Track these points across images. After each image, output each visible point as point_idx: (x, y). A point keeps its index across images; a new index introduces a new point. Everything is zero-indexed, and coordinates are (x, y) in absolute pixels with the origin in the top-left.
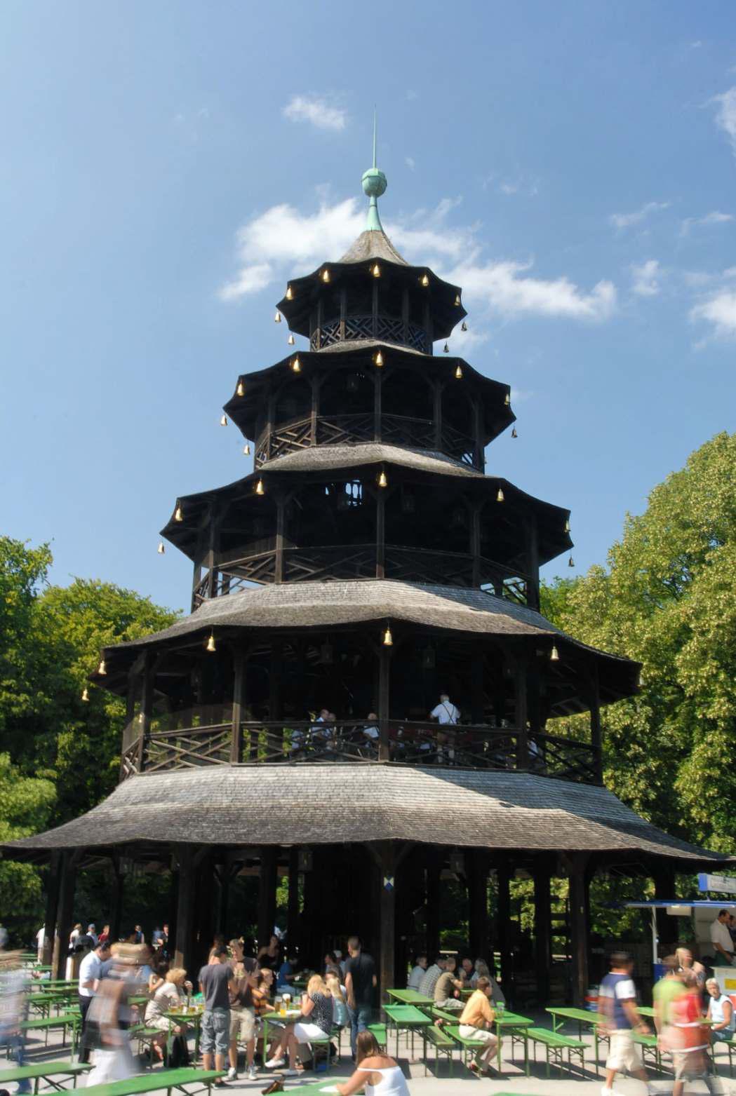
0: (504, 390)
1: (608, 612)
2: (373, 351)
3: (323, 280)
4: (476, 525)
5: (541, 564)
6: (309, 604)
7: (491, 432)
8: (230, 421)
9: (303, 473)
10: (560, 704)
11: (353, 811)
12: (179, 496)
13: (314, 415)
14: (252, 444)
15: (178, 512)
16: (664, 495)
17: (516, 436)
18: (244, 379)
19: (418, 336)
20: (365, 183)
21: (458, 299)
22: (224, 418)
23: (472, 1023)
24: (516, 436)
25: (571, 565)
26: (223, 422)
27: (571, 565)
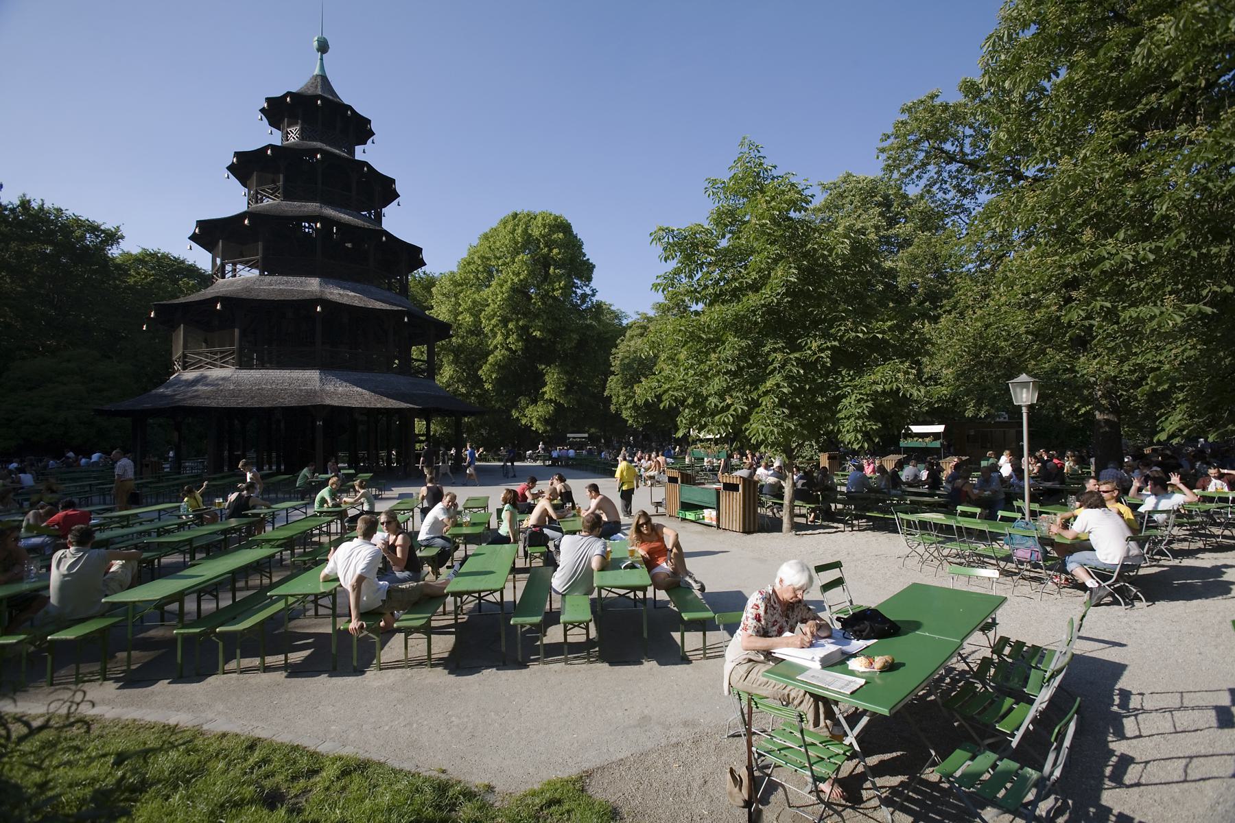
6: (277, 287)
9: (273, 216)
11: (301, 390)
16: (486, 237)
18: (237, 154)
23: (854, 603)
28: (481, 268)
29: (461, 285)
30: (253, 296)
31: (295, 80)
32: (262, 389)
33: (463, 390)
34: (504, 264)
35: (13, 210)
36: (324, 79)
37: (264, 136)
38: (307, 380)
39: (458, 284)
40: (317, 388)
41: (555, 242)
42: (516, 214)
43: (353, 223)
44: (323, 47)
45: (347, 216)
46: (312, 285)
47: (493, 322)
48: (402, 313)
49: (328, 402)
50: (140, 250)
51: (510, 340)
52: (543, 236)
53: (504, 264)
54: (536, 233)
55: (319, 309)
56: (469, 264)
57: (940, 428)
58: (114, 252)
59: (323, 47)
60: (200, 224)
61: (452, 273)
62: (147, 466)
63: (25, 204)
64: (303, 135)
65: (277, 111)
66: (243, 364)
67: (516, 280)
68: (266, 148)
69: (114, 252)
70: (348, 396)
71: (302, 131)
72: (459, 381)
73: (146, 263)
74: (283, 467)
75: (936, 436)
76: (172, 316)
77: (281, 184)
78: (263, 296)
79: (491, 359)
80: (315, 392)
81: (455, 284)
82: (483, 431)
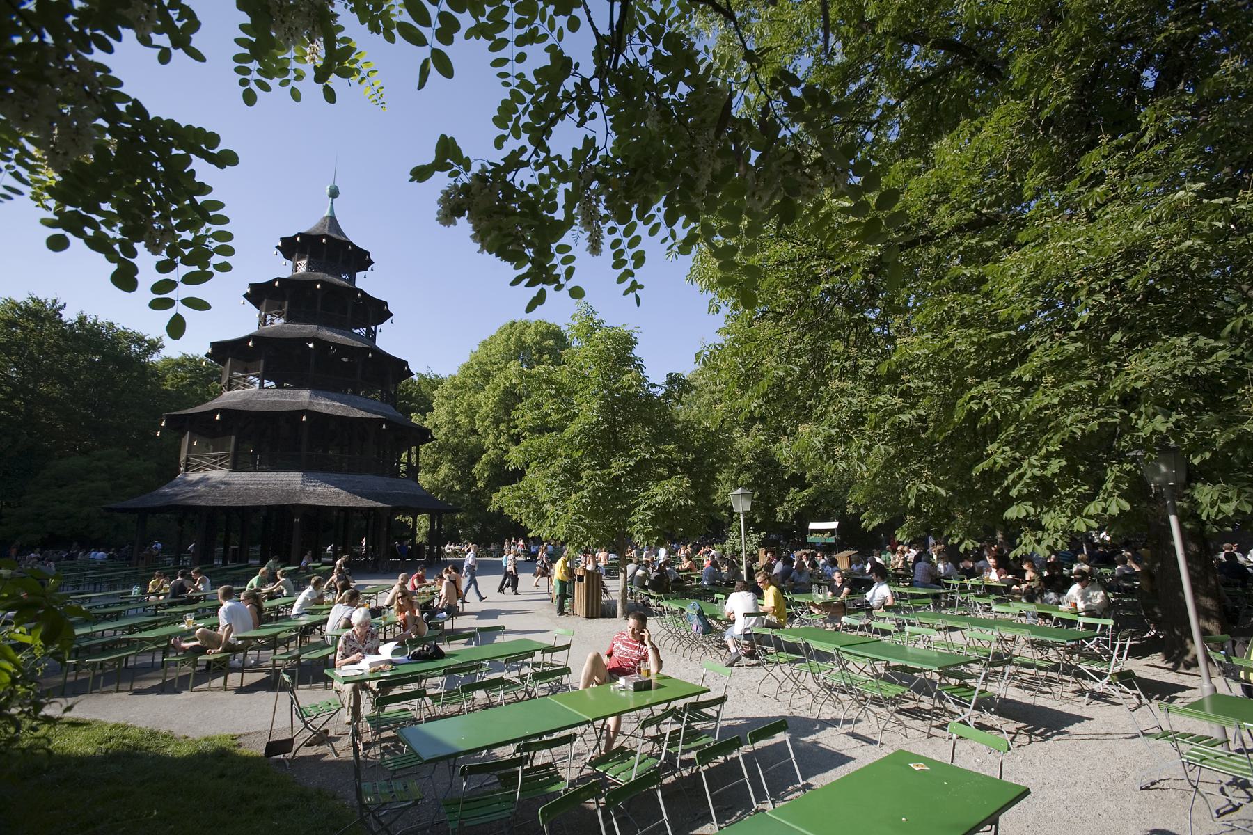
6: (272, 399)
16: (484, 344)
28: (478, 373)
29: (461, 388)
30: (250, 408)
31: (306, 222)
32: (249, 489)
33: (458, 488)
34: (499, 369)
35: (71, 326)
36: (333, 220)
37: (283, 269)
38: (290, 481)
39: (459, 387)
40: (298, 489)
41: (546, 348)
42: (514, 323)
43: (343, 343)
44: (334, 193)
45: (340, 336)
46: (303, 397)
47: (486, 423)
48: (380, 421)
49: (304, 501)
50: (180, 355)
51: (501, 440)
52: (535, 344)
53: (499, 369)
54: (528, 340)
55: (304, 419)
56: (468, 369)
57: (834, 525)
58: (155, 358)
59: (334, 193)
60: (214, 345)
61: (454, 377)
62: (143, 558)
63: (82, 320)
64: (310, 266)
65: (289, 247)
66: (235, 467)
67: (508, 385)
68: (274, 280)
69: (155, 358)
70: (325, 496)
71: (309, 263)
72: (454, 478)
73: (185, 366)
74: (1177, 632)
75: (832, 531)
76: (180, 425)
77: (285, 309)
78: (257, 408)
79: (484, 458)
80: (295, 492)
81: (456, 387)
82: (475, 527)
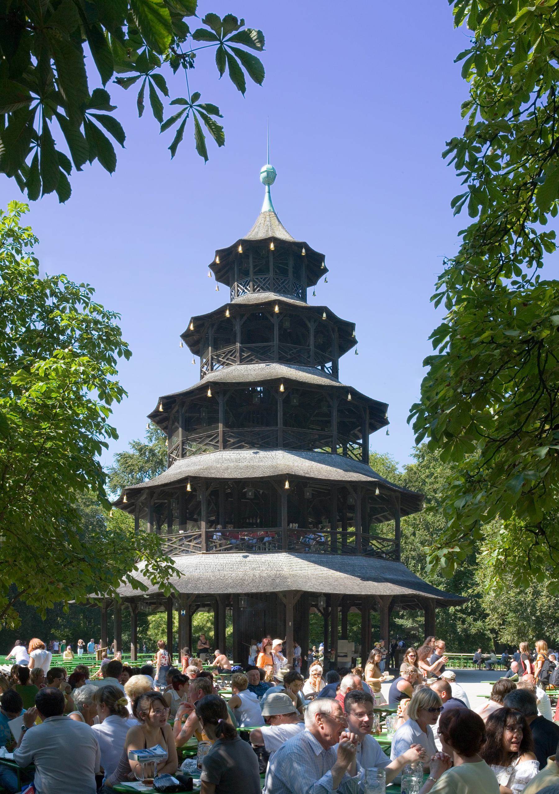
0: (351, 326)
1: (464, 594)
2: (272, 303)
3: (238, 252)
4: (335, 413)
5: (371, 433)
7: (343, 350)
8: (184, 344)
10: (378, 516)
12: (161, 396)
13: (238, 345)
14: (198, 358)
15: (161, 406)
17: (327, 282)
18: (195, 320)
19: (283, 282)
20: (261, 180)
21: (323, 264)
22: (181, 341)
24: (327, 282)
25: (387, 434)
26: (181, 345)
27: (387, 434)
